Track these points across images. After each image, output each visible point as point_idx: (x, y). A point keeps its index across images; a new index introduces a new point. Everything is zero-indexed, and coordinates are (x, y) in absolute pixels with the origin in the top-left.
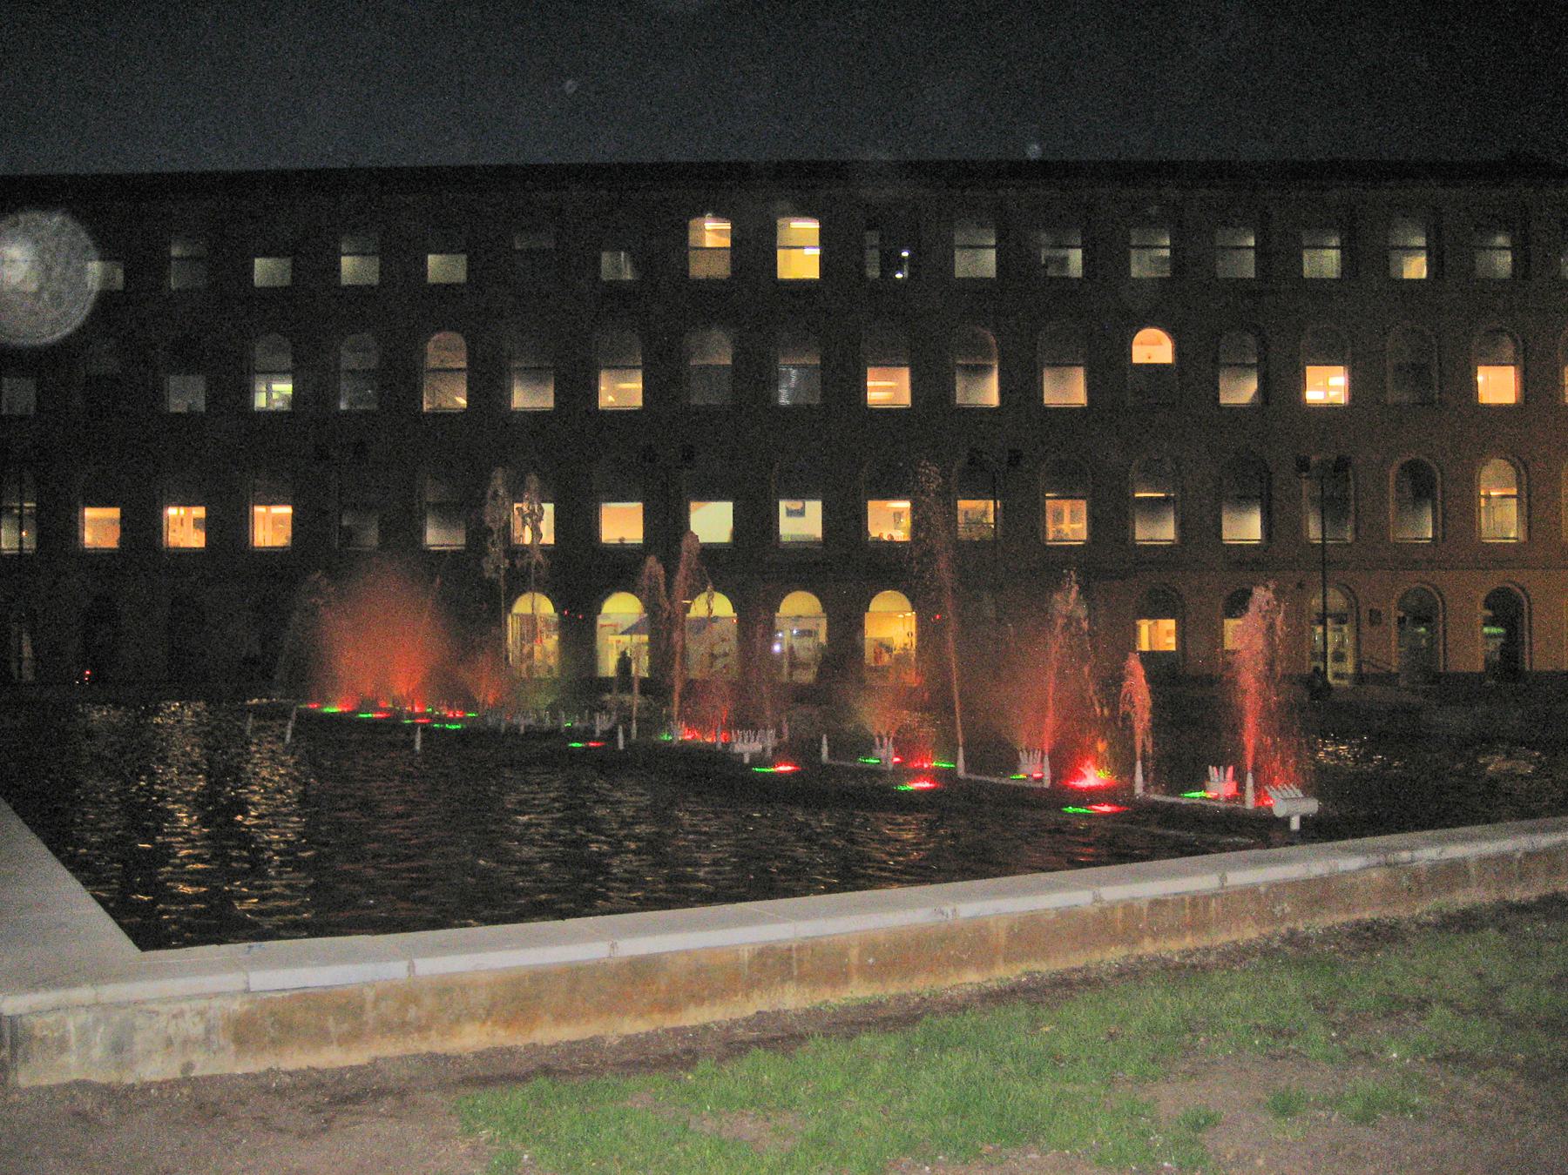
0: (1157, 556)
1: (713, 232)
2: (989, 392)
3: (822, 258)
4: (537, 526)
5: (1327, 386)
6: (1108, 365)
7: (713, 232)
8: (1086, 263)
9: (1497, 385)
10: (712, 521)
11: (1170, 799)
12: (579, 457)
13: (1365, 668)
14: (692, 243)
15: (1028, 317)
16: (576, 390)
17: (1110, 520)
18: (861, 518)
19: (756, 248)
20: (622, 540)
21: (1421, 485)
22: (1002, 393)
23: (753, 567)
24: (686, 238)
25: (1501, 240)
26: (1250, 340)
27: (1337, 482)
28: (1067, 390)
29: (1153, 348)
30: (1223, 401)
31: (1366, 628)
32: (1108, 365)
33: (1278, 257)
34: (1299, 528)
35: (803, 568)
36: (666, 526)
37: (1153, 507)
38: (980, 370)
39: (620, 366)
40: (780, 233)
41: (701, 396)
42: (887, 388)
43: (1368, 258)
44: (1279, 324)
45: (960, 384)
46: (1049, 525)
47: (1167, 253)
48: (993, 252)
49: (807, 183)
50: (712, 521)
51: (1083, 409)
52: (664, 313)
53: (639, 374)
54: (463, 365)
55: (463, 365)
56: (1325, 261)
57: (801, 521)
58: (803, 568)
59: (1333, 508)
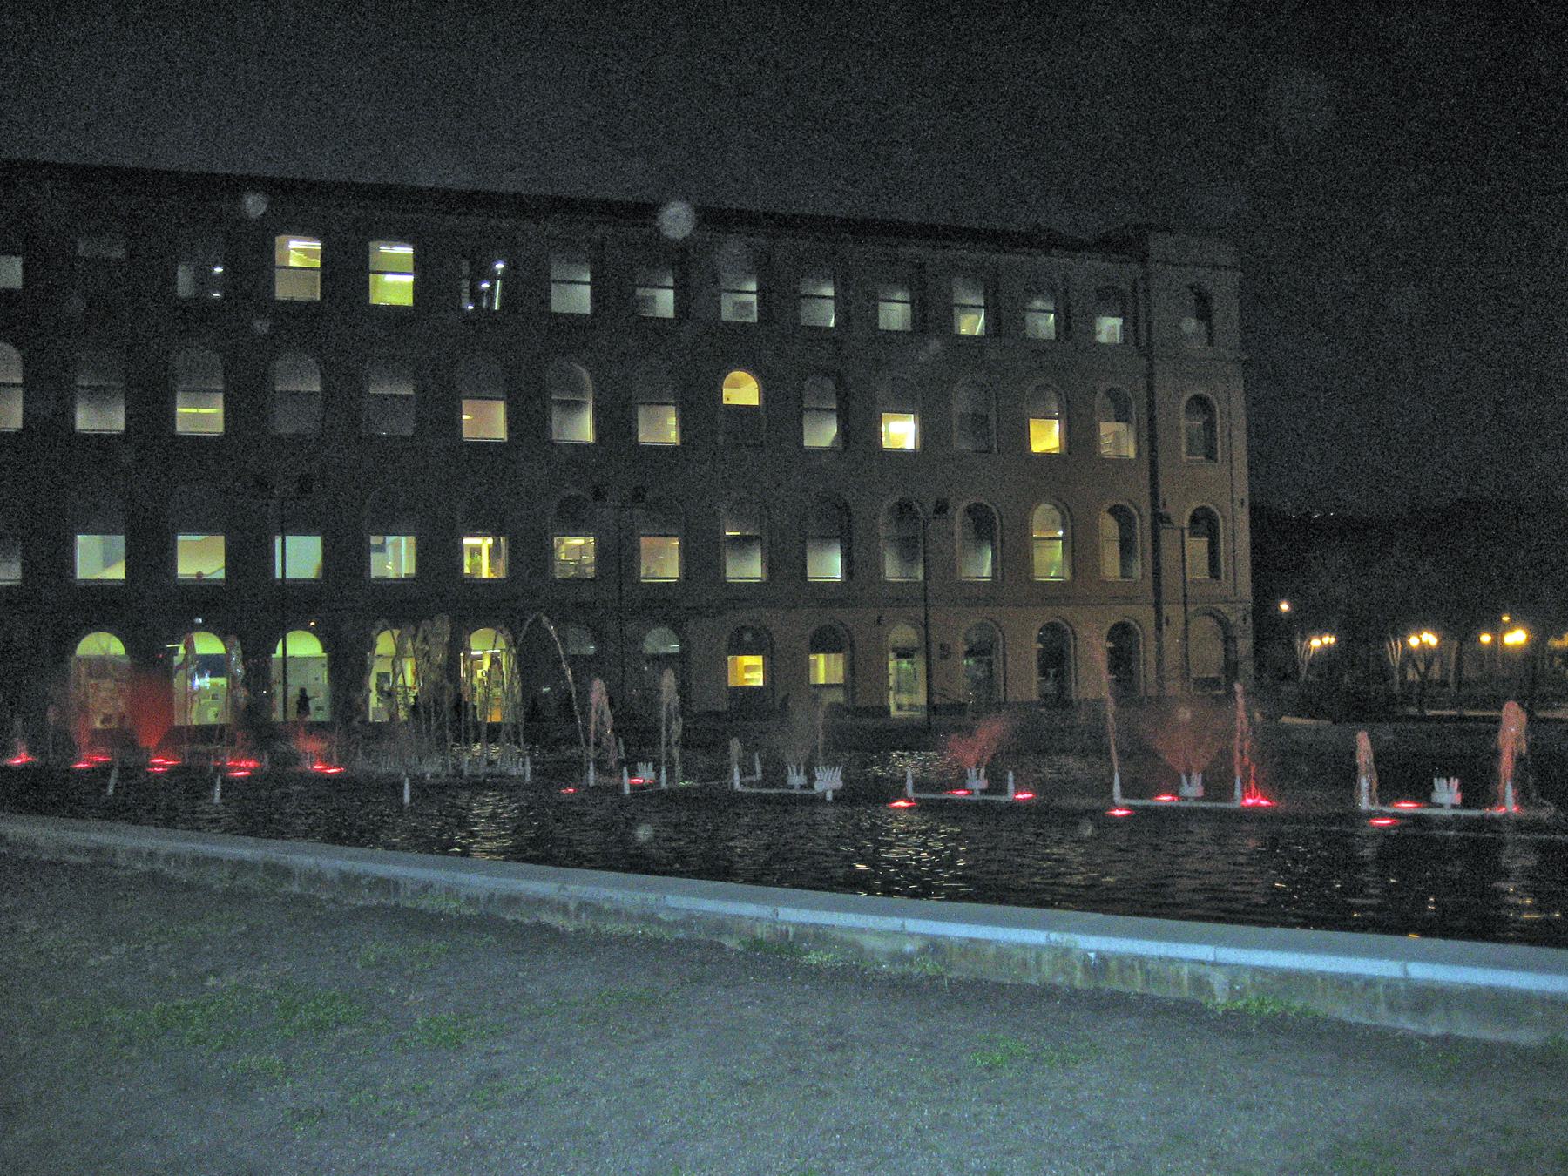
0: (746, 594)
1: (300, 252)
2: (583, 428)
3: (416, 284)
4: (98, 559)
5: (900, 432)
6: (699, 404)
7: (300, 252)
8: (678, 302)
9: (1046, 438)
10: (300, 557)
11: (1506, 765)
12: (152, 486)
13: (937, 701)
14: (278, 262)
15: (621, 351)
16: (151, 409)
17: (703, 558)
18: (266, 556)
19: (346, 271)
20: (199, 575)
21: (983, 525)
22: (597, 426)
23: (345, 606)
24: (272, 260)
25: (899, 296)
26: (830, 385)
27: (915, 524)
28: (662, 428)
29: (743, 391)
30: (807, 443)
31: (938, 665)
32: (699, 404)
33: (857, 309)
34: (878, 567)
35: (399, 605)
36: (346, 557)
37: (742, 543)
38: (575, 406)
39: (201, 392)
40: (372, 258)
41: (285, 424)
42: (485, 421)
43: (932, 316)
44: (854, 375)
45: (556, 416)
46: (467, 561)
47: (753, 298)
48: (587, 289)
49: (395, 209)
50: (300, 557)
51: (675, 448)
52: (246, 332)
53: (220, 398)
54: (19, 380)
55: (19, 380)
56: (895, 314)
57: (395, 558)
58: (399, 605)
59: (909, 549)
